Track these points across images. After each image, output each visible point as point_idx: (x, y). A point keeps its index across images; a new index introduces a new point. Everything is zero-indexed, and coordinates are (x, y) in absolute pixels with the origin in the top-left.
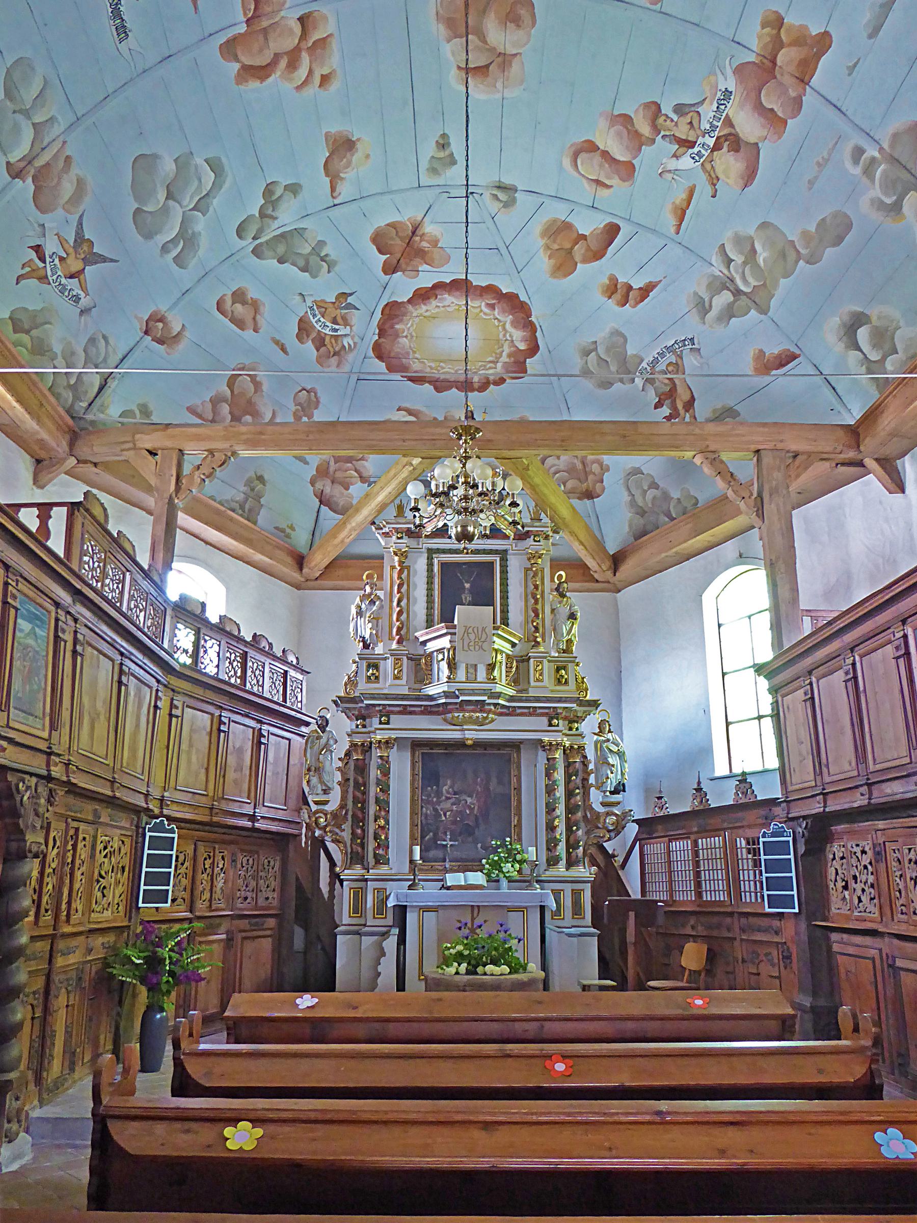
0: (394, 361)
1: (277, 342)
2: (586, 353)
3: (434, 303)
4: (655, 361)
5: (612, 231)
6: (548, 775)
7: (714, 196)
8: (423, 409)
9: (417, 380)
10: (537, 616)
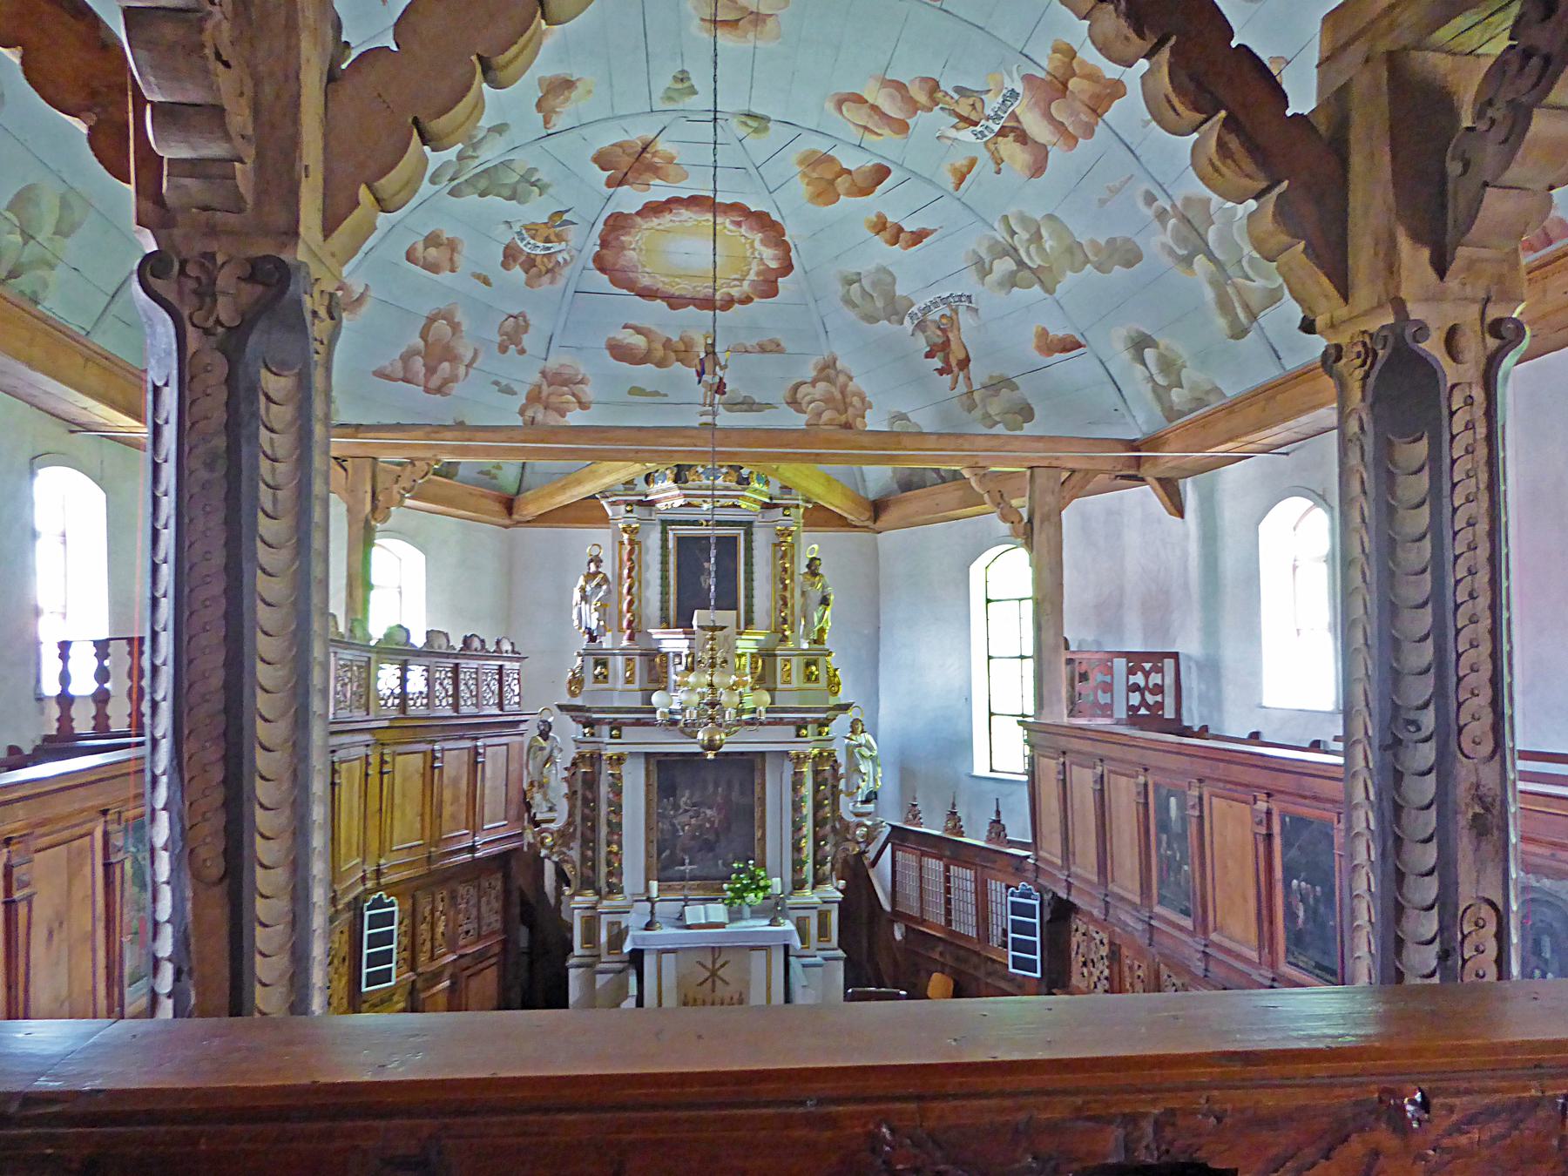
0: (619, 274)
1: (478, 276)
2: (851, 283)
3: (668, 217)
4: (927, 310)
5: (882, 173)
6: (795, 790)
7: (998, 172)
8: (653, 328)
9: (648, 294)
10: (785, 604)
